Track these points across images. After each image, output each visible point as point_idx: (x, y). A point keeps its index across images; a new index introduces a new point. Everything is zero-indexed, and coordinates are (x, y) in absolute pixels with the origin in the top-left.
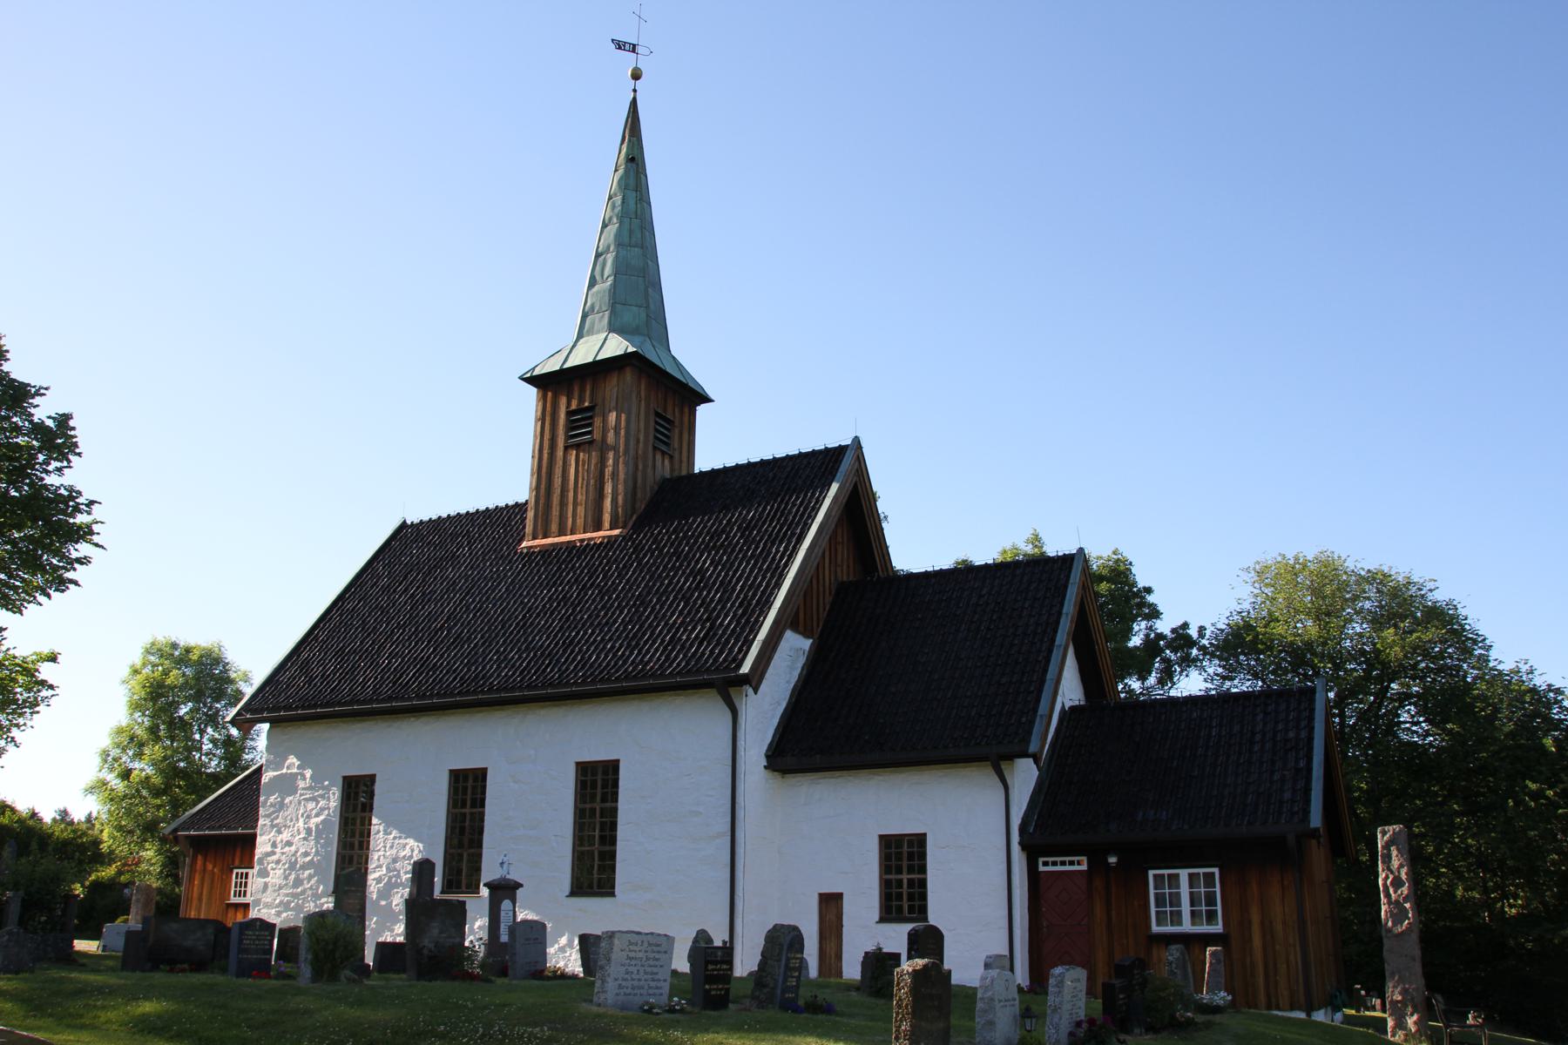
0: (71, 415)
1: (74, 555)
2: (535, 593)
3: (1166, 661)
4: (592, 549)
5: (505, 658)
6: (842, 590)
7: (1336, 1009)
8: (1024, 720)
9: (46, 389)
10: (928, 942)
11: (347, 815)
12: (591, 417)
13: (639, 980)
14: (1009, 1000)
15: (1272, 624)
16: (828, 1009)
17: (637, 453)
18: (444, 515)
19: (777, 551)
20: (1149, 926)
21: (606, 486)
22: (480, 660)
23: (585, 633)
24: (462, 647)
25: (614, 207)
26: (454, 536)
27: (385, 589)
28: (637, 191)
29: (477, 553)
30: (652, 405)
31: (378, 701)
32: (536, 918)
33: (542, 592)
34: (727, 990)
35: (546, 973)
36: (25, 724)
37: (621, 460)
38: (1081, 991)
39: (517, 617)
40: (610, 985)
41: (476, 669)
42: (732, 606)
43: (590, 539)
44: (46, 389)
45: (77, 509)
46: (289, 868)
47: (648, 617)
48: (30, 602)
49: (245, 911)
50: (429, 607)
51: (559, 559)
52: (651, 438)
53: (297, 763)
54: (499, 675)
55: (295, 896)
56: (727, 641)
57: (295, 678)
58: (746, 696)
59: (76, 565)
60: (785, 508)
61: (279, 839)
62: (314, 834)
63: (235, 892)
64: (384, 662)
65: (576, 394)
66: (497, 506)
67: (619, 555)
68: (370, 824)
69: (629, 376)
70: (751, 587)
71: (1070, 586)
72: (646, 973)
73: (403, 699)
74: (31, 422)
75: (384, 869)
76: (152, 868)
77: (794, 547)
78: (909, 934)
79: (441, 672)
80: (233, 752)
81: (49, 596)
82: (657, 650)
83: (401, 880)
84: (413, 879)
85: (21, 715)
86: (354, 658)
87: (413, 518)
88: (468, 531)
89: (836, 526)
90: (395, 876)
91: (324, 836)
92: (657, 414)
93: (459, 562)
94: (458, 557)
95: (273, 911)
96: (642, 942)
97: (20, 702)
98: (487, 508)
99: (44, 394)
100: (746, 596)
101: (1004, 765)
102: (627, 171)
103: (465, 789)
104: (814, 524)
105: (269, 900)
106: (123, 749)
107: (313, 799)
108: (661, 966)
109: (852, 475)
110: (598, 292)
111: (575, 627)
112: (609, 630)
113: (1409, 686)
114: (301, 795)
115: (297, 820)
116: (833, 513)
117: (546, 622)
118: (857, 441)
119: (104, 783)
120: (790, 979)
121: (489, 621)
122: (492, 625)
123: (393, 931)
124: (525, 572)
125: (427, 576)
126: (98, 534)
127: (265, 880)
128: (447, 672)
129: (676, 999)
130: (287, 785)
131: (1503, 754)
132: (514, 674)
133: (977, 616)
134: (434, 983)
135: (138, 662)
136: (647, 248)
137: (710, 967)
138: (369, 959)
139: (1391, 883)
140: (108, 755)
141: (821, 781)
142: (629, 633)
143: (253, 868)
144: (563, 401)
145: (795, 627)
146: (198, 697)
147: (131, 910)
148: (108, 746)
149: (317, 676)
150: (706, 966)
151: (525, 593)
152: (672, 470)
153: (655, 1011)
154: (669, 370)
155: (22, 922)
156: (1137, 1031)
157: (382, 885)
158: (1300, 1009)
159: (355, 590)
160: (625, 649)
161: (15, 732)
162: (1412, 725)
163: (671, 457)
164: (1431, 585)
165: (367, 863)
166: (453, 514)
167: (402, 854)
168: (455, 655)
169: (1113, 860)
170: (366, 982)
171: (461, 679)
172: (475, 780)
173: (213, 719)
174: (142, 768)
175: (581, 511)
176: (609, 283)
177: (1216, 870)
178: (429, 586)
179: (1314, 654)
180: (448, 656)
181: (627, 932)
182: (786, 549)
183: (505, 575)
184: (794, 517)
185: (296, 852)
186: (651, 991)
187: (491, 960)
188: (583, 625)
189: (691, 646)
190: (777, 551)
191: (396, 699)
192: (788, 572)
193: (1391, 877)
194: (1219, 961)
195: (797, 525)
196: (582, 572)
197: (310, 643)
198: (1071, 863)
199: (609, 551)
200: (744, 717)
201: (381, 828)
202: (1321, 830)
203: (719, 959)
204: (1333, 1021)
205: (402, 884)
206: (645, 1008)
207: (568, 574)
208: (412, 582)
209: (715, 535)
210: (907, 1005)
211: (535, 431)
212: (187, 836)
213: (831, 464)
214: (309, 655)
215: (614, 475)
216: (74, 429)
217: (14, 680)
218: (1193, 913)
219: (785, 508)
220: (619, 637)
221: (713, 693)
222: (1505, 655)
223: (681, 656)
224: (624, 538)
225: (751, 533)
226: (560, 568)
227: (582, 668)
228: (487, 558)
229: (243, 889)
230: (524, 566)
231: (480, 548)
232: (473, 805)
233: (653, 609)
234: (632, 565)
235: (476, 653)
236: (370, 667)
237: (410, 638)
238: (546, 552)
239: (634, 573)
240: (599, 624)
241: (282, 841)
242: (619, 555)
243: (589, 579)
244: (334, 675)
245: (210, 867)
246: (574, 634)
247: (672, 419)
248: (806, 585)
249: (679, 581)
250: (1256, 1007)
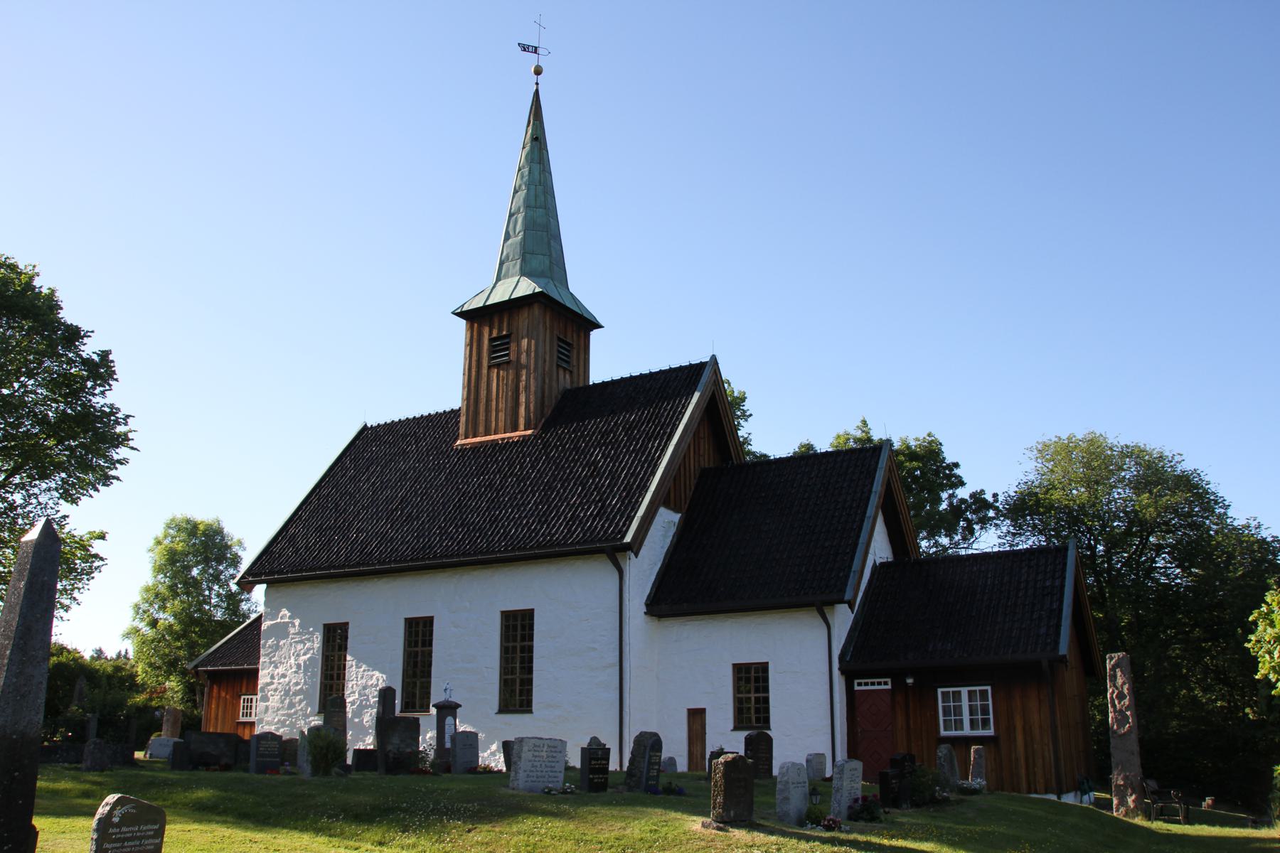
0: (110, 351)
1: (116, 457)
2: (467, 481)
3: (969, 522)
4: (511, 445)
5: (446, 532)
6: (704, 474)
7: (1084, 792)
8: (841, 574)
9: (92, 332)
10: (760, 746)
11: (327, 654)
12: (508, 343)
13: (542, 771)
14: (800, 783)
15: (1051, 491)
16: (680, 792)
17: (544, 371)
18: (396, 420)
19: (653, 446)
20: (938, 732)
21: (521, 397)
22: (427, 534)
23: (506, 512)
24: (412, 524)
25: (522, 177)
26: (405, 436)
27: (352, 479)
28: (540, 163)
29: (422, 450)
30: (555, 332)
31: (350, 567)
32: (473, 730)
33: (473, 480)
34: (606, 779)
35: (479, 769)
36: (83, 588)
37: (532, 376)
38: (858, 777)
39: (454, 500)
40: (521, 775)
41: (424, 540)
42: (618, 489)
43: (509, 438)
44: (92, 332)
45: (117, 422)
46: (284, 695)
47: (554, 499)
48: (84, 495)
49: (251, 729)
50: (387, 492)
51: (485, 454)
52: (555, 357)
53: (289, 614)
54: (441, 545)
55: (289, 716)
56: (615, 517)
57: (285, 549)
58: (630, 559)
59: (118, 465)
60: (659, 412)
61: (276, 673)
62: (302, 668)
63: (243, 713)
64: (353, 536)
65: (496, 325)
66: (437, 412)
67: (531, 451)
68: (345, 660)
69: (536, 310)
70: (632, 475)
71: (878, 470)
72: (546, 766)
73: (368, 565)
74: (81, 357)
75: (357, 694)
76: (175, 696)
77: (666, 443)
78: (746, 738)
79: (397, 543)
80: (232, 601)
81: (97, 490)
82: (561, 525)
83: (370, 702)
84: (379, 702)
85: (81, 580)
86: (330, 533)
87: (372, 422)
88: (415, 432)
89: (699, 424)
90: (365, 700)
91: (310, 670)
92: (559, 339)
93: (408, 457)
94: (408, 453)
96: (544, 745)
97: (79, 571)
98: (429, 414)
99: (90, 336)
100: (629, 482)
101: (827, 610)
102: (532, 148)
103: (417, 633)
104: (681, 425)
105: (270, 719)
106: (150, 603)
107: (302, 642)
108: (558, 762)
109: (710, 385)
110: (511, 244)
111: (499, 507)
112: (525, 510)
113: (1164, 538)
114: (292, 639)
115: (290, 658)
116: (696, 416)
117: (477, 504)
118: (714, 359)
119: (137, 631)
120: (652, 771)
121: (432, 503)
122: (435, 506)
123: (364, 741)
124: (460, 464)
125: (384, 468)
126: (133, 439)
127: (265, 704)
128: (401, 544)
129: (567, 784)
130: (281, 631)
131: (1236, 592)
132: (452, 544)
133: (807, 494)
134: (398, 776)
135: (160, 534)
136: (549, 208)
137: (593, 762)
138: (349, 761)
139: (1117, 696)
140: (140, 608)
141: (689, 623)
142: (539, 512)
143: (257, 694)
144: (486, 331)
145: (667, 505)
146: (206, 561)
147: (163, 728)
148: (139, 601)
149: (301, 548)
150: (590, 762)
151: (460, 481)
152: (572, 382)
153: (553, 792)
154: (568, 305)
155: (99, 735)
156: (905, 806)
157: (355, 707)
158: (1052, 792)
159: (329, 479)
160: (537, 525)
161: (76, 594)
162: (1166, 568)
163: (571, 372)
164: (1177, 458)
165: (343, 690)
166: (403, 418)
167: (370, 683)
168: (407, 530)
169: (910, 681)
170: (350, 776)
171: (412, 549)
172: (425, 626)
173: (216, 578)
174: (166, 618)
175: (502, 416)
176: (520, 237)
177: (989, 688)
178: (386, 476)
179: (1086, 515)
180: (402, 531)
181: (533, 738)
182: (659, 444)
183: (445, 467)
184: (665, 421)
185: (289, 682)
186: (550, 779)
187: (439, 761)
188: (505, 505)
189: (587, 521)
190: (653, 446)
191: (363, 565)
192: (661, 463)
193: (1116, 692)
194: (980, 756)
195: (668, 425)
196: (503, 464)
197: (296, 521)
198: (879, 684)
199: (524, 447)
200: (628, 575)
201: (354, 663)
202: (1068, 657)
203: (600, 756)
204: (1081, 802)
205: (370, 706)
206: (546, 790)
207: (492, 466)
208: (372, 473)
209: (605, 434)
210: (721, 785)
211: (465, 354)
212: (205, 671)
213: (694, 377)
214: (295, 531)
215: (527, 388)
216: (112, 361)
217: (74, 555)
218: (972, 721)
219: (659, 412)
220: (532, 515)
221: (604, 557)
222: (1239, 515)
223: (580, 529)
224: (535, 436)
225: (632, 432)
226: (486, 460)
227: (504, 540)
228: (430, 453)
229: (249, 711)
230: (459, 459)
231: (425, 446)
232: (424, 645)
233: (558, 492)
234: (541, 458)
235: (423, 528)
236: (341, 540)
237: (372, 517)
238: (475, 448)
239: (543, 464)
240: (517, 504)
241: (278, 674)
242: (531, 451)
243: (509, 470)
244: (315, 546)
245: (223, 694)
246: (497, 512)
247: (571, 342)
248: (675, 471)
249: (577, 471)
250: (1019, 791)
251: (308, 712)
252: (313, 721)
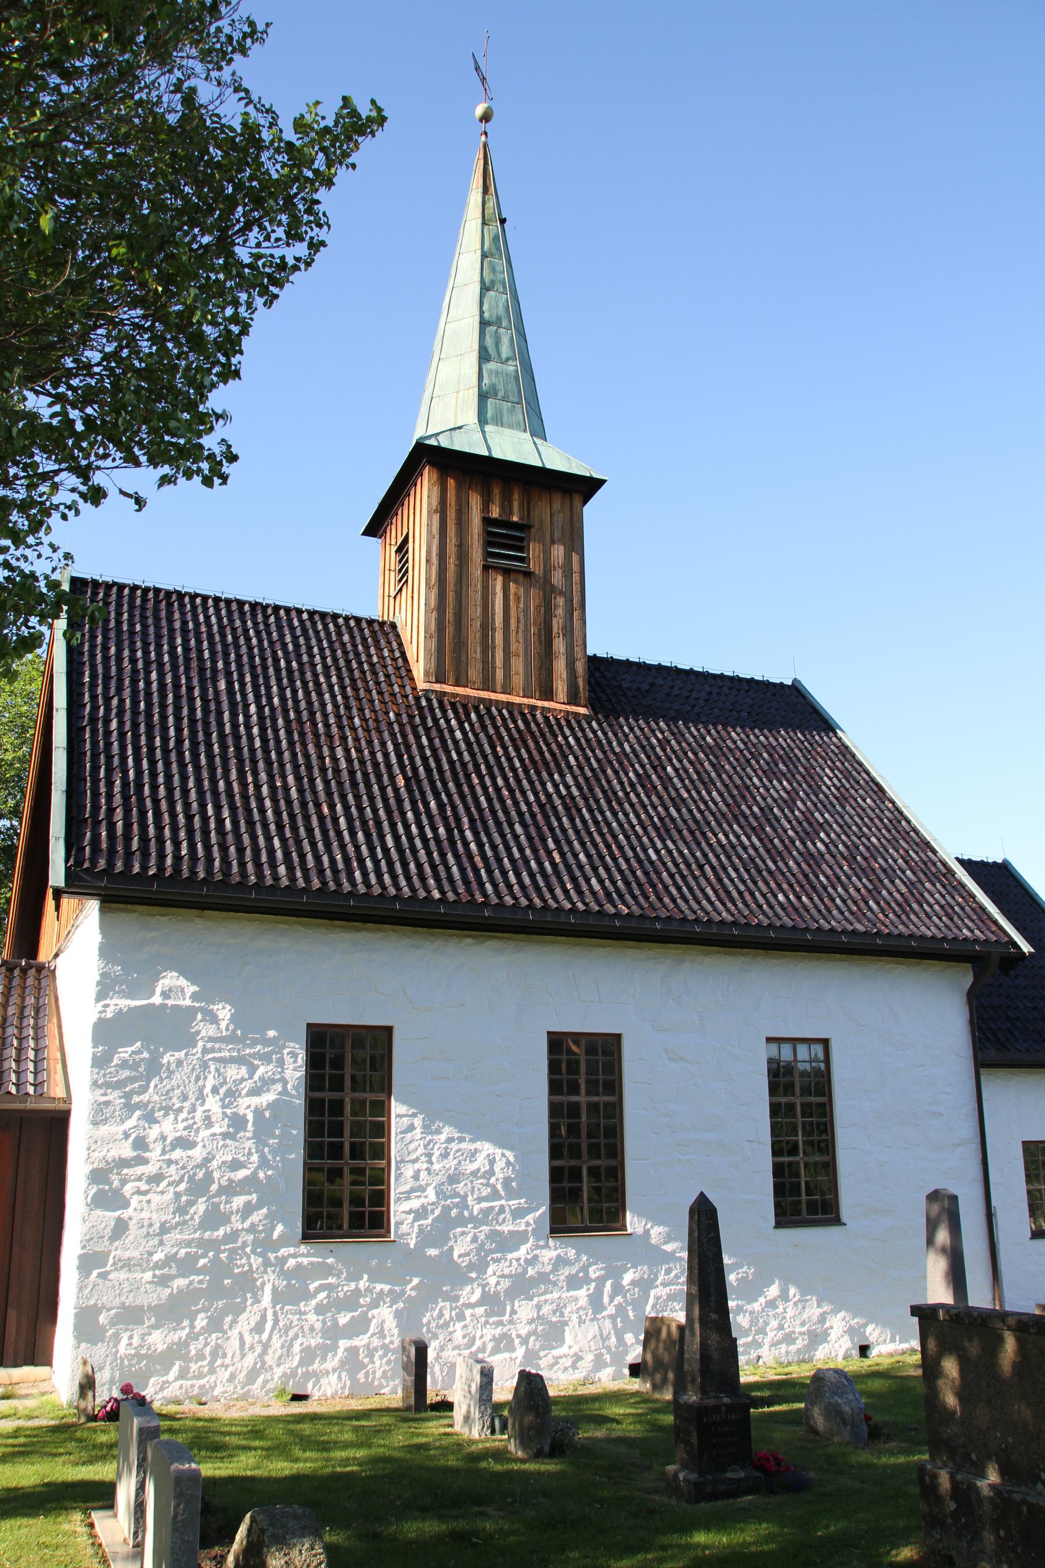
83: (471, 1213)
90: (456, 1206)
95: (148, 1276)
107: (240, 1061)
115: (201, 1098)
144: (475, 502)
157: (429, 1221)
167: (472, 1167)
201: (418, 1122)
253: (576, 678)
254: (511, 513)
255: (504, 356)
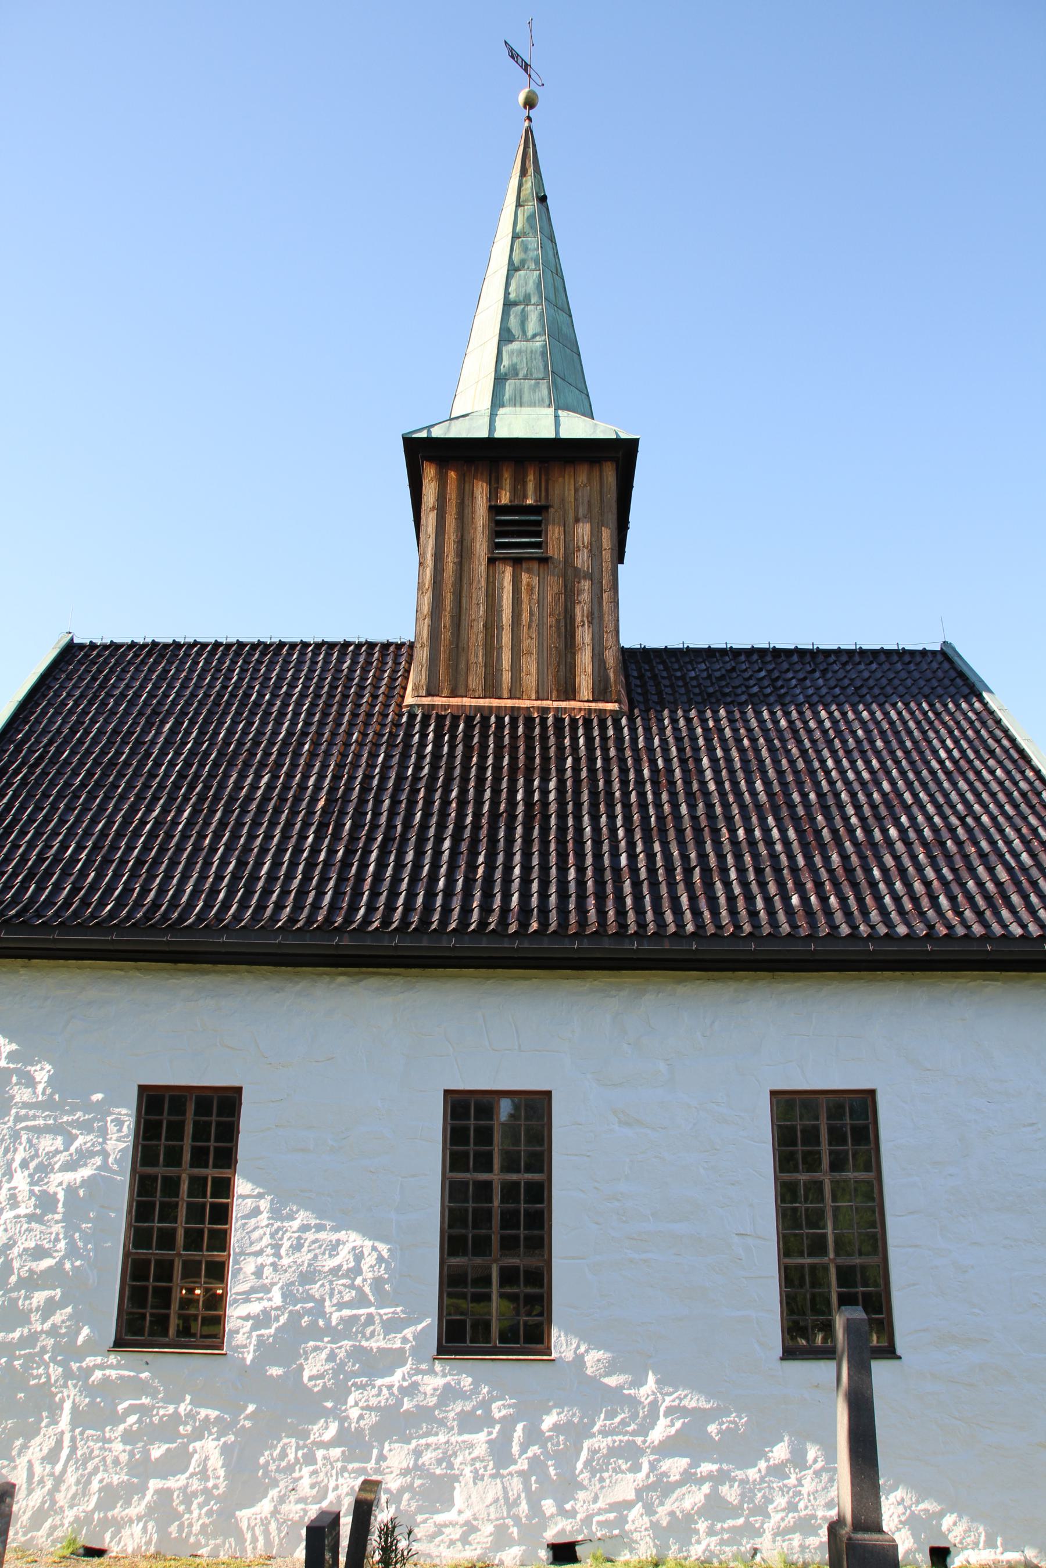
62: (60, 1208)
90: (308, 1312)
107: (55, 1130)
114: (18, 1119)
201: (264, 1204)
232: (199, 1158)
251: (80, 1340)
252: (97, 1367)
253: (606, 669)
254: (525, 497)
255: (530, 333)
